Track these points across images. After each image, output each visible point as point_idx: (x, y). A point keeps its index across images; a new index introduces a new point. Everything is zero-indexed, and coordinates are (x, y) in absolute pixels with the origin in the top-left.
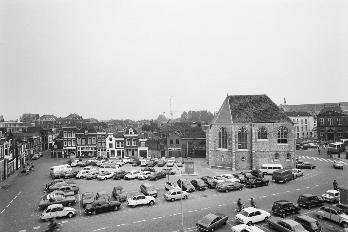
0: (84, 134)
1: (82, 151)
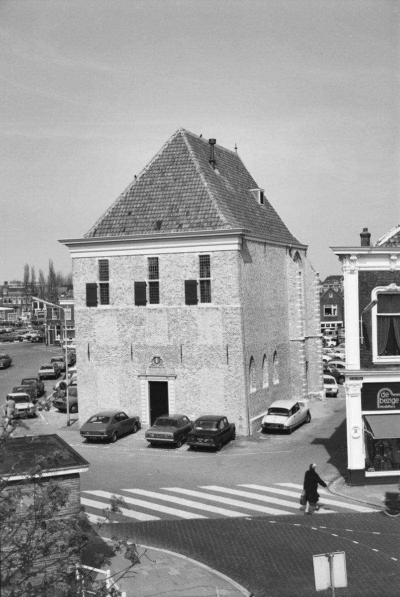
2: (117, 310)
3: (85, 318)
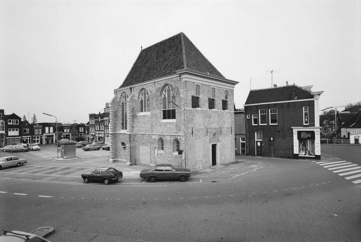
0: (98, 120)
1: (98, 136)
2: (203, 111)
3: (191, 114)
